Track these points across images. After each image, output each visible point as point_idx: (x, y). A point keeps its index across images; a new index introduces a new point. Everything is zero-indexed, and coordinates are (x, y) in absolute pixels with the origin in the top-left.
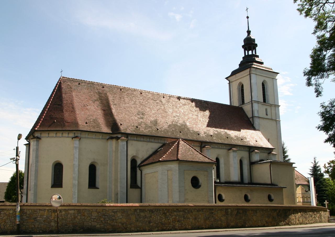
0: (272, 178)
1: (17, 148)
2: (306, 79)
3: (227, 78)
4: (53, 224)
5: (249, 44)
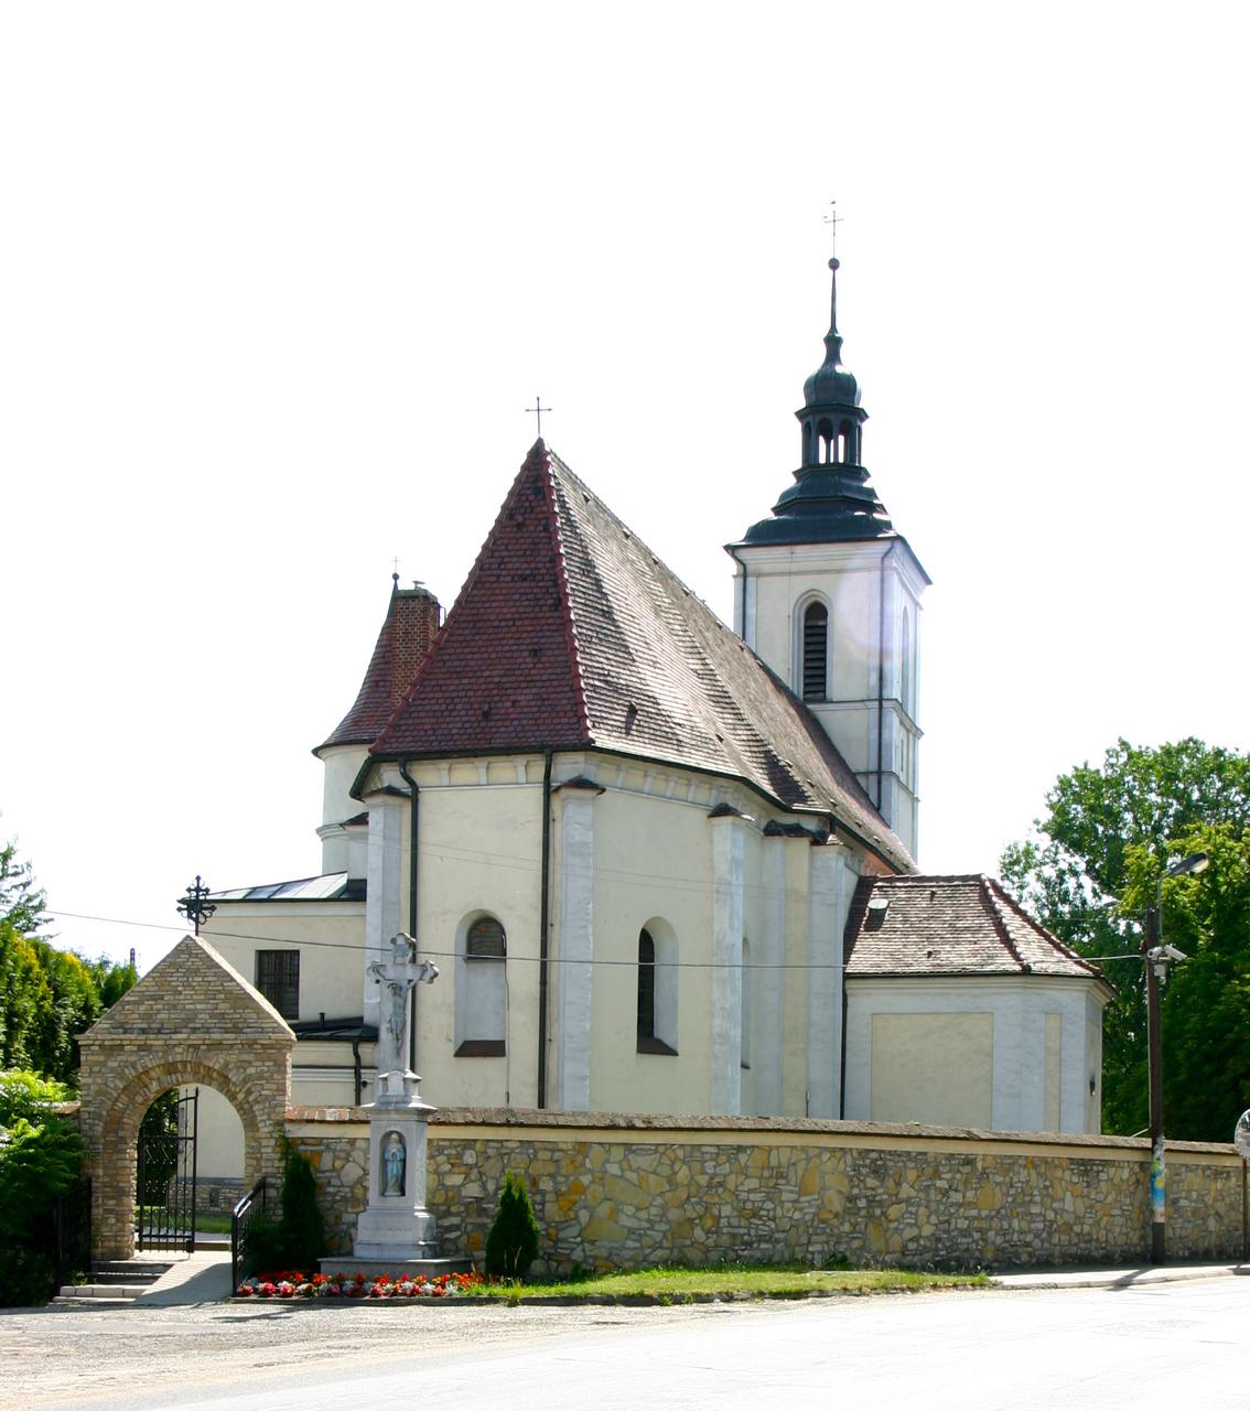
0: (407, 845)
1: (905, 608)
2: (1168, 743)
3: (731, 549)
4: (1212, 1224)
5: (832, 407)
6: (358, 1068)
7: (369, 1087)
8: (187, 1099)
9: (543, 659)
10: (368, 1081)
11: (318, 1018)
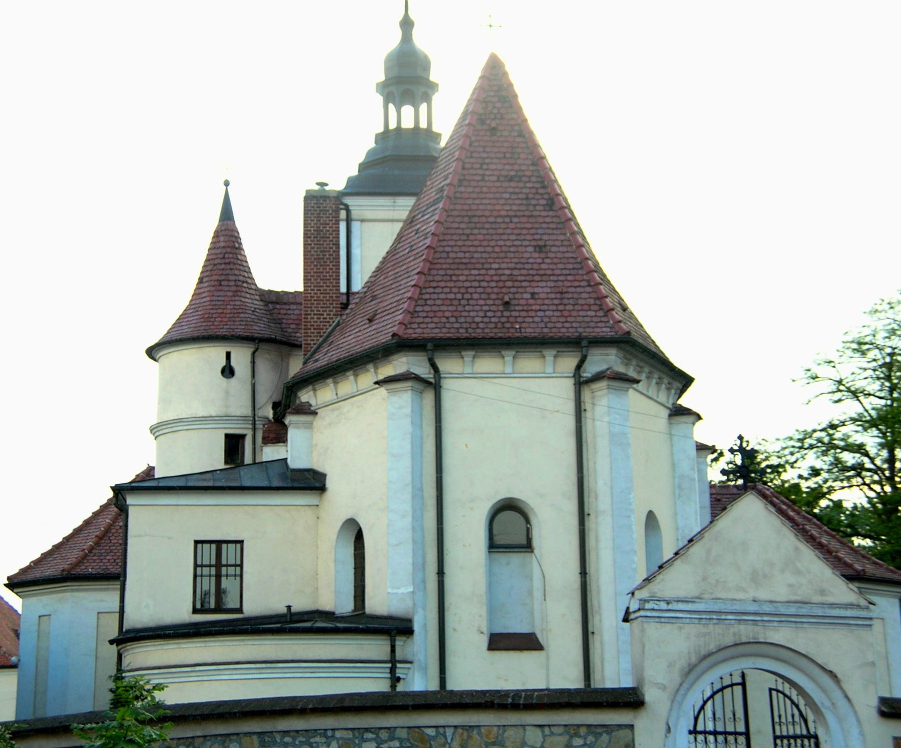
6: (393, 661)
7: (402, 681)
8: (732, 685)
9: (551, 255)
10: (401, 676)
11: (285, 610)
